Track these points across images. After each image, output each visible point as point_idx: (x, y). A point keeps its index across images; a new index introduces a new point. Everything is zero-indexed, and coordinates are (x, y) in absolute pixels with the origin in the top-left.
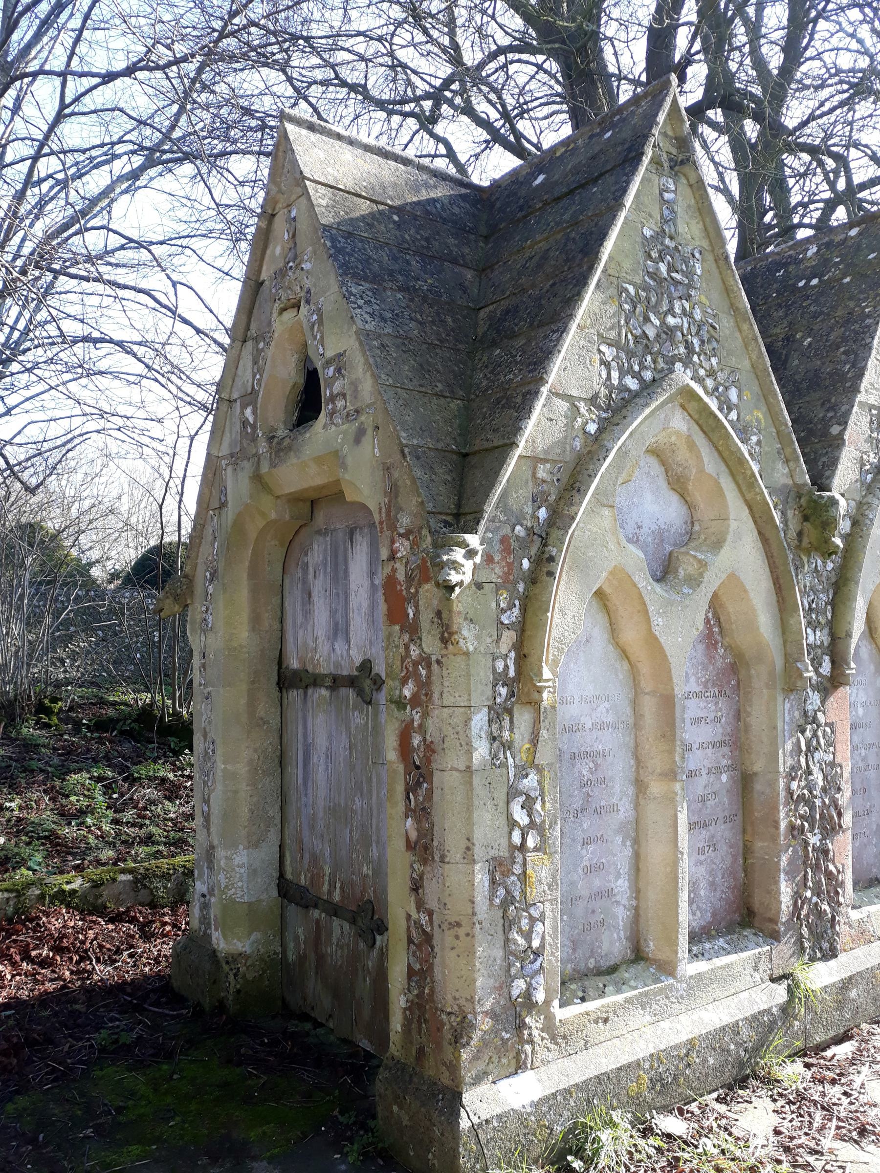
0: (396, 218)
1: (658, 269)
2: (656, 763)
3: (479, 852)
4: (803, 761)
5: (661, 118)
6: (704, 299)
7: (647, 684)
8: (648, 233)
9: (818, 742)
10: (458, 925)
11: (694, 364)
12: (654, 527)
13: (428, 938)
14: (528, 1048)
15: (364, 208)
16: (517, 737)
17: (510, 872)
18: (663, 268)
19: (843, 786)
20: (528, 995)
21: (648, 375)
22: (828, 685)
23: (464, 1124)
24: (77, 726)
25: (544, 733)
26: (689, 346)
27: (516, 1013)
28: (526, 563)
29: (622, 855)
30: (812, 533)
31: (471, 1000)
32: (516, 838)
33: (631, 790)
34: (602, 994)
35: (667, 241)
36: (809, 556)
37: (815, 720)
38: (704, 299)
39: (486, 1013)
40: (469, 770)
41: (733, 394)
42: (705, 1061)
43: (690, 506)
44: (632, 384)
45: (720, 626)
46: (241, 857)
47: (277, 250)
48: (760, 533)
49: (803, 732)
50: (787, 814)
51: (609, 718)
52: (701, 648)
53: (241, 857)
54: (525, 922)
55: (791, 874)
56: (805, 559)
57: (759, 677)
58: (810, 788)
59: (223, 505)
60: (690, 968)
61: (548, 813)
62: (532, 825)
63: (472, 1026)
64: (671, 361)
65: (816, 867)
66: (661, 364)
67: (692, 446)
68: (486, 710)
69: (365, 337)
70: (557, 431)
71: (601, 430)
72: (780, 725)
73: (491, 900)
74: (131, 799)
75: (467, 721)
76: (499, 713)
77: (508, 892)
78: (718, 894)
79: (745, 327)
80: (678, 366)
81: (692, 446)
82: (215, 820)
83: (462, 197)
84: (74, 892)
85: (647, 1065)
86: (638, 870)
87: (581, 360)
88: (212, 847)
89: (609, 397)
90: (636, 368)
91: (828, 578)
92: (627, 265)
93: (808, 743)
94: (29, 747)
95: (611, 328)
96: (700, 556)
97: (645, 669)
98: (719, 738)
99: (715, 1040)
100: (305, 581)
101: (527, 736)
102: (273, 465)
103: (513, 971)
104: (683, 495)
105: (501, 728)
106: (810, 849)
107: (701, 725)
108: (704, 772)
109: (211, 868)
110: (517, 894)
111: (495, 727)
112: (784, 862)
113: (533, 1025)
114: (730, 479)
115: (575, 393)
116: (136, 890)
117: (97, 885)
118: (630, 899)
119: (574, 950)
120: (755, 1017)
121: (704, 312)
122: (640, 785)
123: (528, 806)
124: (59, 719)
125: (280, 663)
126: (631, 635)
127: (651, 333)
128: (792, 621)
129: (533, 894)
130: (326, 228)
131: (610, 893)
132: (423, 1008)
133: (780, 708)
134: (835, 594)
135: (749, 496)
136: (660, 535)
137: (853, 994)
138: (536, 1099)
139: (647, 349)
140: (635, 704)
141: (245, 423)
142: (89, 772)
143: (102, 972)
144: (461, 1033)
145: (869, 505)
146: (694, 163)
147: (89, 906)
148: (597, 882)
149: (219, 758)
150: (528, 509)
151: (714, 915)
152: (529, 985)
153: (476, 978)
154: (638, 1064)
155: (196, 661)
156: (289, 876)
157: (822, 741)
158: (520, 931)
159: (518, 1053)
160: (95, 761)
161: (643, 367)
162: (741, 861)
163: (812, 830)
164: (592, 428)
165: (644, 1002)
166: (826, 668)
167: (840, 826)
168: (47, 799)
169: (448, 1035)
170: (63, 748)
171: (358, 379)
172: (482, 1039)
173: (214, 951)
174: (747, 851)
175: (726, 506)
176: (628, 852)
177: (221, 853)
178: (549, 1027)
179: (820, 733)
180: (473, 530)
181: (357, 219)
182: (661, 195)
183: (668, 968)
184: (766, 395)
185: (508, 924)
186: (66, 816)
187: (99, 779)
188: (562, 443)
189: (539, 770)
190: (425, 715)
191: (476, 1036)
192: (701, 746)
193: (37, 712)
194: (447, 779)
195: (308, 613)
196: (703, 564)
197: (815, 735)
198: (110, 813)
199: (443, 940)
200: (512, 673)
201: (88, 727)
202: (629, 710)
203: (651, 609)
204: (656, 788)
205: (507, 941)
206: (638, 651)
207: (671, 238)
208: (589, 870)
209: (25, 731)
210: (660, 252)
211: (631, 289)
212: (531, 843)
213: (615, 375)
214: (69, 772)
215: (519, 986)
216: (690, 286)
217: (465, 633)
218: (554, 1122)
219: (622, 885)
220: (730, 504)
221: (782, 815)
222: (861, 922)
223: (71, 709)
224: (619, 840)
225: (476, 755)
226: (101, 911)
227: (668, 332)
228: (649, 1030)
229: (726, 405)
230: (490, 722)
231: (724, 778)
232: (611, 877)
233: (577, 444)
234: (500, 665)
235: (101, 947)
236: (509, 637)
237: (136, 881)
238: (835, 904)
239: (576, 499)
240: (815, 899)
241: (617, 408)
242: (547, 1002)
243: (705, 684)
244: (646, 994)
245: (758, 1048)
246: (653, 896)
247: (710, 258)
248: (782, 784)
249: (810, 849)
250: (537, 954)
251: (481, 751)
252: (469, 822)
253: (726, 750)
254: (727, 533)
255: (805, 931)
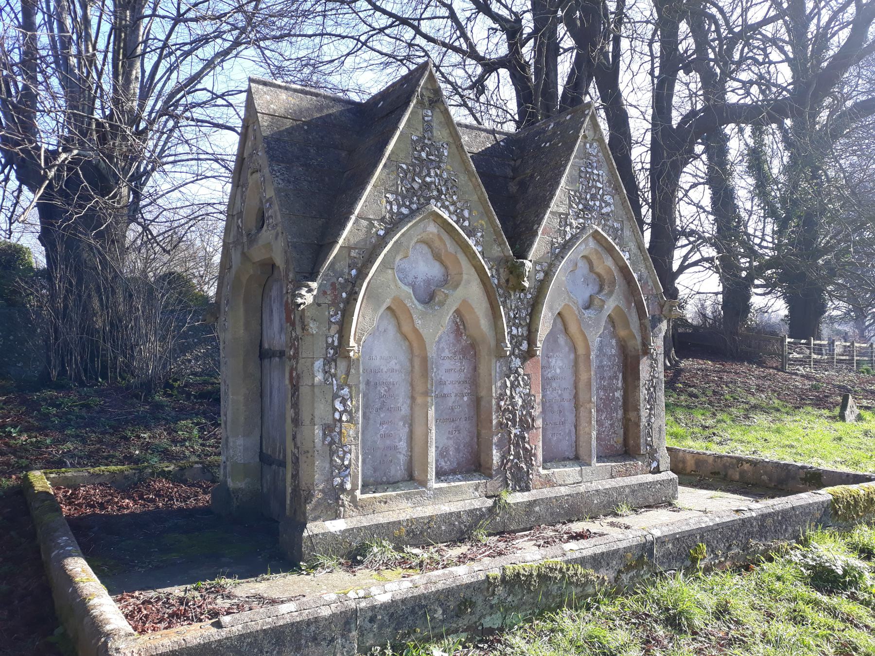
0: (306, 127)
1: (420, 155)
2: (420, 388)
3: (317, 420)
4: (508, 392)
5: (422, 83)
6: (449, 167)
7: (417, 352)
8: (415, 138)
9: (519, 383)
10: (308, 452)
11: (442, 200)
12: (424, 278)
13: (297, 459)
14: (342, 509)
15: (288, 124)
16: (339, 372)
17: (332, 430)
18: (424, 155)
19: (536, 406)
20: (342, 485)
21: (414, 206)
22: (526, 355)
23: (305, 534)
24: (189, 395)
25: (353, 371)
26: (440, 192)
27: (335, 493)
28: (344, 295)
29: (404, 432)
30: (513, 281)
31: (313, 484)
32: (337, 416)
33: (409, 401)
34: (385, 491)
35: (426, 141)
36: (515, 291)
37: (517, 372)
38: (449, 167)
39: (320, 491)
40: (313, 385)
41: (466, 213)
42: (440, 527)
43: (446, 268)
44: (405, 211)
45: (464, 325)
46: (240, 441)
47: (249, 144)
48: (481, 280)
49: (509, 377)
50: (497, 417)
51: (397, 367)
52: (452, 336)
53: (240, 441)
54: (341, 453)
55: (500, 446)
56: (512, 293)
57: (484, 352)
58: (514, 405)
59: (231, 267)
60: (434, 484)
61: (354, 406)
62: (345, 411)
63: (313, 496)
64: (428, 200)
65: (517, 445)
66: (422, 200)
67: (441, 239)
68: (322, 360)
69: (278, 191)
70: (361, 235)
71: (386, 234)
72: (493, 374)
73: (323, 442)
74: (214, 434)
75: (313, 364)
76: (328, 361)
77: (332, 439)
78: (461, 455)
79: (474, 179)
80: (433, 201)
81: (441, 239)
82: (229, 424)
83: (348, 110)
84: (170, 471)
85: (405, 524)
86: (411, 438)
87: (375, 201)
88: (228, 437)
89: (391, 218)
90: (408, 203)
91: (528, 302)
92: (402, 155)
93: (512, 383)
94: (158, 406)
95: (393, 185)
96: (446, 292)
97: (415, 345)
98: (463, 379)
99: (447, 518)
100: (271, 305)
101: (344, 372)
102: (249, 249)
103: (334, 474)
104: (442, 262)
105: (330, 368)
106: (512, 436)
107: (449, 372)
108: (453, 395)
109: (227, 448)
110: (337, 440)
111: (327, 367)
112: (495, 439)
113: (345, 499)
114: (463, 255)
115: (371, 217)
116: (204, 473)
117: (182, 469)
118: (407, 451)
119: (375, 472)
120: (471, 511)
121: (449, 174)
122: (413, 398)
123: (344, 402)
124: (179, 392)
125: (261, 345)
126: (406, 329)
127: (416, 186)
128: (499, 323)
129: (345, 440)
130: (265, 138)
131: (396, 448)
132: (296, 490)
133: (493, 365)
134: (532, 310)
135: (474, 262)
136: (428, 282)
137: (537, 509)
138: (342, 529)
139: (414, 194)
140: (411, 361)
141: (238, 227)
142: (191, 420)
143: (177, 504)
144: (309, 496)
145: (555, 265)
146: (442, 101)
147: (177, 478)
148: (388, 442)
149: (230, 393)
150: (346, 270)
151: (458, 464)
152: (343, 481)
153: (317, 475)
154: (399, 522)
155: (221, 343)
156: (264, 451)
157: (521, 383)
158: (338, 457)
159: (336, 510)
160: (197, 414)
161: (411, 203)
162: (476, 440)
163: (514, 426)
164: (382, 233)
165: (408, 497)
166: (525, 346)
167: (533, 426)
168: (165, 433)
169: (303, 500)
170: (179, 407)
171: (275, 213)
172: (317, 501)
173: (228, 489)
174: (479, 435)
175: (461, 267)
176: (407, 429)
177: (231, 440)
178: (354, 500)
179: (520, 379)
180: (314, 280)
181: (283, 131)
182: (423, 118)
183: (424, 483)
184: (487, 212)
185: (332, 453)
186: (174, 442)
187: (197, 424)
188: (365, 240)
189: (350, 387)
190: (297, 363)
191: (314, 500)
192: (452, 382)
193: (165, 388)
194: (304, 390)
195: (271, 321)
196: (446, 295)
197: (516, 379)
198: (200, 441)
199: (302, 458)
200: (336, 344)
201: (195, 397)
202: (408, 364)
203: (414, 316)
204: (419, 400)
205: (332, 460)
206: (411, 336)
207: (429, 139)
208: (383, 436)
209: (157, 398)
210: (422, 147)
211: (404, 166)
212: (344, 418)
213: (395, 208)
214: (180, 420)
215: (338, 480)
216: (440, 162)
217: (311, 325)
218: (352, 541)
219: (403, 445)
220: (463, 267)
221: (494, 417)
222: (547, 476)
223: (186, 386)
224: (401, 423)
225: (317, 379)
226: (185, 482)
227: (427, 186)
228: (410, 510)
229: (460, 219)
230: (324, 365)
231: (465, 399)
232: (397, 441)
233: (373, 240)
234: (330, 340)
235: (180, 495)
236: (334, 329)
237: (204, 467)
238: (530, 465)
239: (369, 266)
240: (516, 461)
241: (394, 224)
242: (353, 490)
243: (455, 353)
244: (409, 493)
245: (474, 525)
246: (417, 449)
247: (454, 147)
248: (494, 402)
249: (512, 436)
250: (347, 467)
251: (319, 377)
252: (313, 408)
253: (468, 386)
254: (461, 280)
255: (509, 475)
